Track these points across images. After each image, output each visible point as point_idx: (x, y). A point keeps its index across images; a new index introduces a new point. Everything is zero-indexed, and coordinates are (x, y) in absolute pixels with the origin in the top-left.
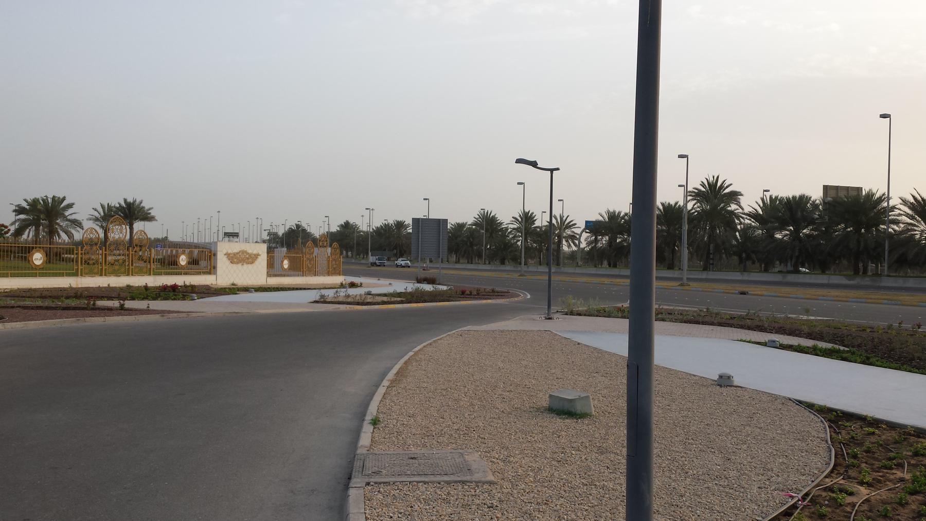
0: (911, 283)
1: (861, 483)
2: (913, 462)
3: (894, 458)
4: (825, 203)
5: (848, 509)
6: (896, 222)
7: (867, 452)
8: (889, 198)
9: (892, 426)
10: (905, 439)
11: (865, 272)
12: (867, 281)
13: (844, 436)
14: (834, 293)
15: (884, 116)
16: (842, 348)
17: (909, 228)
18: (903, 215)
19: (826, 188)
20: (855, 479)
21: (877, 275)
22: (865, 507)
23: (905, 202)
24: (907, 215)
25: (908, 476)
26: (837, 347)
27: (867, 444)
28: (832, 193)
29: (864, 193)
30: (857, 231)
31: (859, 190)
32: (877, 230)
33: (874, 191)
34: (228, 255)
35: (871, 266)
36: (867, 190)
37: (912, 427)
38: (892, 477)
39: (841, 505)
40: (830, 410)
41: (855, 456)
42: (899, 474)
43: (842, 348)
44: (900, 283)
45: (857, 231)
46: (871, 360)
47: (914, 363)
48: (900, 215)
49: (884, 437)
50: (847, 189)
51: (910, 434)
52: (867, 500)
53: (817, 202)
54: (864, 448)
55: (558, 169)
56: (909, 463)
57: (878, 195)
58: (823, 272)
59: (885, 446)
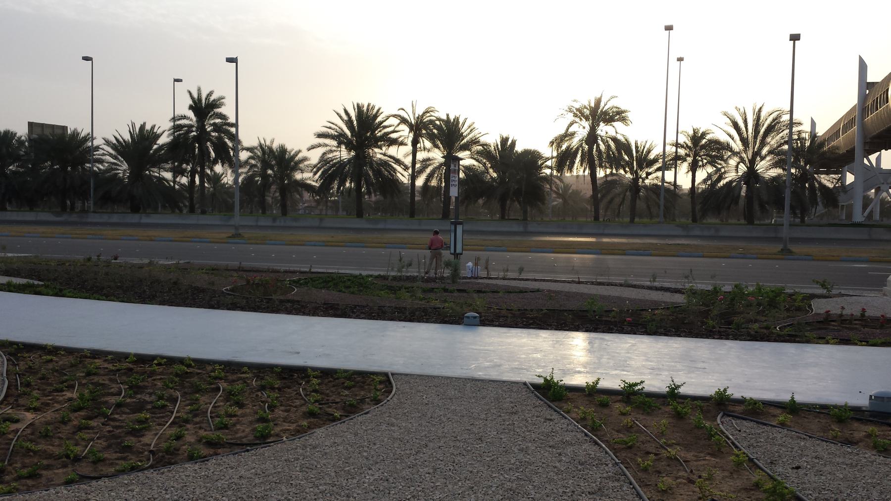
0: (115, 218)
1: (28, 410)
2: (84, 382)
3: (65, 382)
4: (30, 140)
5: (11, 436)
6: (101, 161)
7: (41, 379)
8: (93, 139)
9: (70, 351)
10: (81, 362)
11: (73, 208)
12: (74, 218)
13: (22, 366)
14: (41, 229)
15: (86, 59)
16: (36, 282)
17: (112, 167)
18: (106, 154)
19: (31, 125)
20: (23, 406)
21: (84, 211)
22: (29, 431)
23: (108, 143)
24: (111, 155)
25: (75, 395)
26: (31, 281)
27: (43, 371)
28: (38, 131)
29: (69, 132)
30: (64, 168)
31: (64, 128)
32: (83, 169)
33: (79, 130)
34: (402, 144)
35: (79, 204)
36: (73, 129)
37: (88, 350)
38: (61, 398)
39: (4, 434)
40: (12, 344)
41: (28, 385)
42: (69, 395)
43: (36, 282)
44: (105, 218)
45: (64, 168)
46: (64, 292)
47: (105, 291)
48: (104, 155)
49: (61, 363)
50: (53, 127)
51: (86, 357)
52: (31, 424)
53: (23, 138)
54: (39, 375)
55: (863, 67)
56: (80, 384)
57: (83, 135)
58: (31, 210)
59: (60, 371)
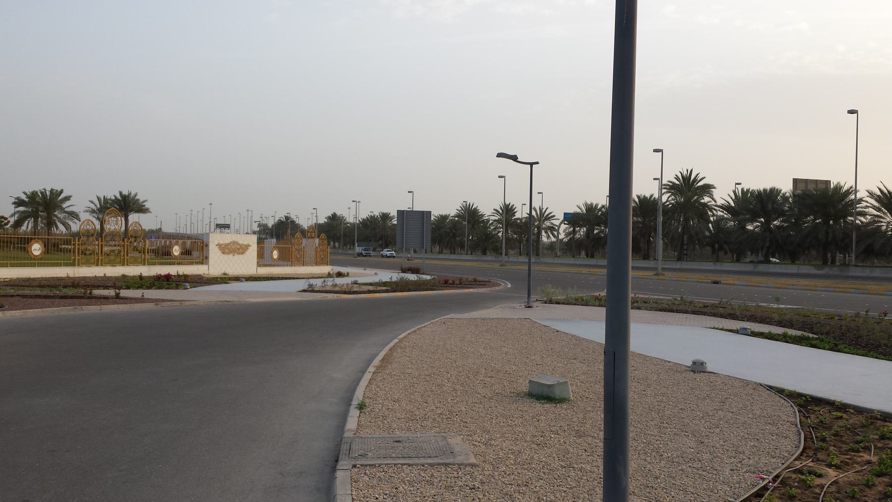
0: (877, 273)
1: (830, 466)
2: (879, 445)
3: (861, 442)
4: (794, 195)
5: (817, 491)
6: (863, 214)
7: (835, 435)
8: (856, 191)
9: (859, 410)
10: (872, 423)
11: (833, 262)
12: (835, 271)
13: (813, 420)
14: (804, 282)
15: (851, 112)
16: (811, 335)
17: (876, 219)
18: (869, 207)
19: (795, 181)
20: (823, 461)
21: (844, 265)
22: (833, 489)
23: (871, 195)
24: (874, 207)
25: (874, 459)
26: (806, 334)
27: (835, 427)
28: (802, 186)
29: (832, 186)
30: (826, 222)
31: (828, 183)
32: (845, 222)
33: (842, 184)
34: (219, 245)
35: (839, 256)
36: (835, 183)
37: (878, 411)
38: (859, 459)
39: (810, 487)
40: (800, 395)
41: (823, 440)
42: (866, 457)
43: (811, 335)
44: (867, 272)
45: (826, 222)
46: (839, 347)
47: (880, 350)
48: (867, 207)
49: (851, 421)
50: (816, 182)
51: (876, 419)
52: (835, 482)
53: (787, 194)
54: (833, 432)
55: (537, 163)
56: (875, 447)
57: (845, 188)
58: (793, 262)
59: (852, 430)
